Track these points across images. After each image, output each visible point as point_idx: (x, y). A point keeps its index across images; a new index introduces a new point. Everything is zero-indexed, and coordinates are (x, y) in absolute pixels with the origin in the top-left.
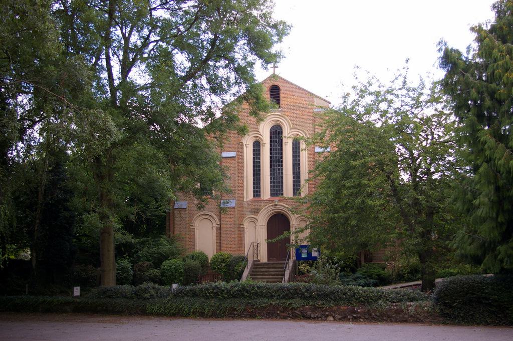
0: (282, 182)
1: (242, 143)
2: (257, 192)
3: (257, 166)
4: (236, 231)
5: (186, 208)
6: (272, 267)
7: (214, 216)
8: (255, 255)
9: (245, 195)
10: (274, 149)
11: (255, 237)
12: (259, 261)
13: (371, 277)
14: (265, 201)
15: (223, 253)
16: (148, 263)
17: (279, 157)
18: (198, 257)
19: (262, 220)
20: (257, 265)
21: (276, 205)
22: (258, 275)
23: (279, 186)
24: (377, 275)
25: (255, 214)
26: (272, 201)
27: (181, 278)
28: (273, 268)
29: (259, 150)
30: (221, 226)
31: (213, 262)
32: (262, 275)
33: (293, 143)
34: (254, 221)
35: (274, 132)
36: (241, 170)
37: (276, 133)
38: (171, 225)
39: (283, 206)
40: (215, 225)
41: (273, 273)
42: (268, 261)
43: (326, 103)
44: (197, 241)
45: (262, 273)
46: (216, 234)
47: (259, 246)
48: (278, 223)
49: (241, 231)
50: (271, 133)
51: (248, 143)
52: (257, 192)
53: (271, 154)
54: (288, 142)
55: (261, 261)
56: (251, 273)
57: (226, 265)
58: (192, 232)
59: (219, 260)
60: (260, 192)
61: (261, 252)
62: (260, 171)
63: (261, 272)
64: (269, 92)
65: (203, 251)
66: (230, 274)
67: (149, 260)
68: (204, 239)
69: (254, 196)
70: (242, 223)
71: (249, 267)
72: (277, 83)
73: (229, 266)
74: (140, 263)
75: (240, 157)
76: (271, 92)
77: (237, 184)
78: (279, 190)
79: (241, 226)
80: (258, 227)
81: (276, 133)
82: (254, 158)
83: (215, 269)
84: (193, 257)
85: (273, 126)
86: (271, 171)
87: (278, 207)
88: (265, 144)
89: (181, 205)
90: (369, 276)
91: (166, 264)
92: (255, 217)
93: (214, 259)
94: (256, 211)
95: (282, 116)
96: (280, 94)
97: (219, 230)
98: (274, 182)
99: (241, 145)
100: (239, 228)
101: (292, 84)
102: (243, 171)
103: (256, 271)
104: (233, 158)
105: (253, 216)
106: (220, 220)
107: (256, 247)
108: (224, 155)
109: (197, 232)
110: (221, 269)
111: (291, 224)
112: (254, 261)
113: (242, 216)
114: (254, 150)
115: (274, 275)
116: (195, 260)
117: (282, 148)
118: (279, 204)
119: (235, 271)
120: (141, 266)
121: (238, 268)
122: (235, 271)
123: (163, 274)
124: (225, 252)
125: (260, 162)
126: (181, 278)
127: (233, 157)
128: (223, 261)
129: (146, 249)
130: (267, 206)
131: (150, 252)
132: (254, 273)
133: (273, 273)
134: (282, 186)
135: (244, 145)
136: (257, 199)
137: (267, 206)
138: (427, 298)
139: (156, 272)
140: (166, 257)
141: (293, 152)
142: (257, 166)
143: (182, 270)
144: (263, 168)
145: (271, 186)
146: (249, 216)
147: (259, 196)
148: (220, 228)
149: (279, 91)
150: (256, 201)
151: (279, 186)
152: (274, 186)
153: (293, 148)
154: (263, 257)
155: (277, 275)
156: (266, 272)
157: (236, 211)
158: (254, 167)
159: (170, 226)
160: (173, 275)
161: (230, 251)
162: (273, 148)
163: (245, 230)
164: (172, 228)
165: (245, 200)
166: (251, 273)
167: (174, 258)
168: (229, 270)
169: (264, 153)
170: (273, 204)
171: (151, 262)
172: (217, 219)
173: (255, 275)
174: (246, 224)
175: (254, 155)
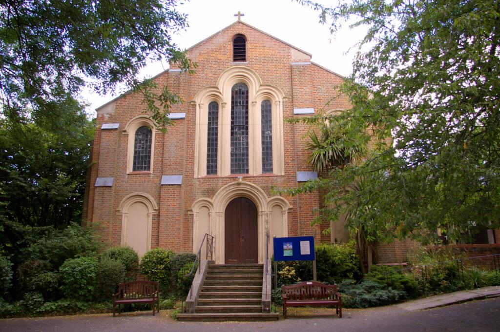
0: (247, 155)
1: (194, 102)
2: (212, 167)
3: (213, 134)
4: (182, 220)
5: (111, 187)
6: (238, 272)
7: (151, 198)
8: (209, 255)
9: (196, 169)
10: (236, 117)
11: (208, 229)
12: (214, 262)
13: (392, 285)
14: (223, 178)
15: (160, 249)
16: (41, 262)
17: (243, 122)
18: (121, 254)
19: (219, 203)
20: (212, 268)
21: (239, 184)
22: (218, 284)
23: (243, 160)
24: (402, 283)
25: (209, 196)
26: (235, 179)
27: (90, 288)
28: (238, 272)
29: (217, 113)
30: (159, 213)
31: (145, 263)
32: (223, 284)
33: (262, 106)
34: (207, 206)
35: (236, 92)
36: (190, 137)
37: (240, 94)
38: (90, 211)
39: (250, 185)
40: (151, 211)
41: (241, 281)
42: (225, 263)
43: (307, 56)
44: (124, 232)
45: (222, 281)
46: (153, 223)
47: (214, 241)
48: (242, 213)
49: (188, 218)
50: (233, 92)
51: (202, 103)
52: (212, 167)
53: (232, 118)
54: (256, 102)
55: (216, 263)
56: (205, 280)
57: (164, 268)
58: (117, 217)
59: (155, 260)
60: (216, 167)
61: (217, 249)
62: (216, 139)
63: (221, 278)
64: (232, 43)
65: (131, 247)
66: (170, 282)
67: (44, 258)
68: (136, 232)
69: (208, 173)
70: (189, 209)
71: (202, 271)
72: (243, 32)
73: (169, 269)
74: (28, 262)
75: (191, 121)
76: (234, 42)
77: (185, 155)
78: (244, 165)
79: (189, 213)
80: (213, 214)
81: (240, 94)
82: (209, 123)
83: (147, 273)
84: (113, 255)
85: (237, 84)
86: (232, 140)
87: (242, 187)
88: (226, 103)
89: (105, 182)
90: (389, 285)
91: (68, 265)
92: (209, 200)
93: (146, 258)
94: (211, 192)
95: (249, 70)
96: (246, 45)
97: (157, 217)
98: (236, 155)
99: (193, 105)
100: (186, 215)
101: (262, 33)
102: (194, 139)
103: (214, 278)
104: (181, 121)
105: (206, 199)
106: (159, 204)
107: (210, 240)
108: (171, 116)
109: (125, 221)
110: (156, 274)
111: (260, 210)
112: (209, 262)
113: (190, 199)
114: (209, 113)
115: (242, 284)
116: (116, 259)
117: (248, 132)
118: (244, 182)
119: (179, 276)
120: (27, 266)
121: (184, 273)
122: (179, 276)
123: (60, 282)
124: (165, 250)
125: (217, 129)
126: (90, 288)
127: (182, 119)
128: (161, 261)
129: (42, 241)
130: (227, 185)
131: (49, 246)
132: (208, 281)
133: (241, 281)
134: (247, 160)
135: (197, 106)
136: (211, 176)
137: (227, 185)
138: (28, 239)
139: (50, 276)
140: (72, 253)
141: (263, 116)
142: (213, 138)
143: (93, 275)
144: (222, 135)
145: (232, 160)
146: (201, 199)
147: (216, 172)
148: (159, 215)
149: (245, 42)
150: (211, 178)
151: (243, 154)
152: (236, 160)
153: (262, 112)
154: (220, 258)
155: (248, 284)
156: (229, 278)
157: (183, 191)
158: (209, 134)
159: (87, 212)
160: (76, 283)
161: (171, 248)
162: (235, 110)
163: (195, 218)
164: (89, 215)
165: (196, 176)
166: (205, 280)
167: (84, 256)
168: (169, 275)
169: (224, 115)
170: (236, 182)
171: (48, 261)
172: (155, 203)
173: (211, 284)
174: (196, 209)
175: (209, 119)
